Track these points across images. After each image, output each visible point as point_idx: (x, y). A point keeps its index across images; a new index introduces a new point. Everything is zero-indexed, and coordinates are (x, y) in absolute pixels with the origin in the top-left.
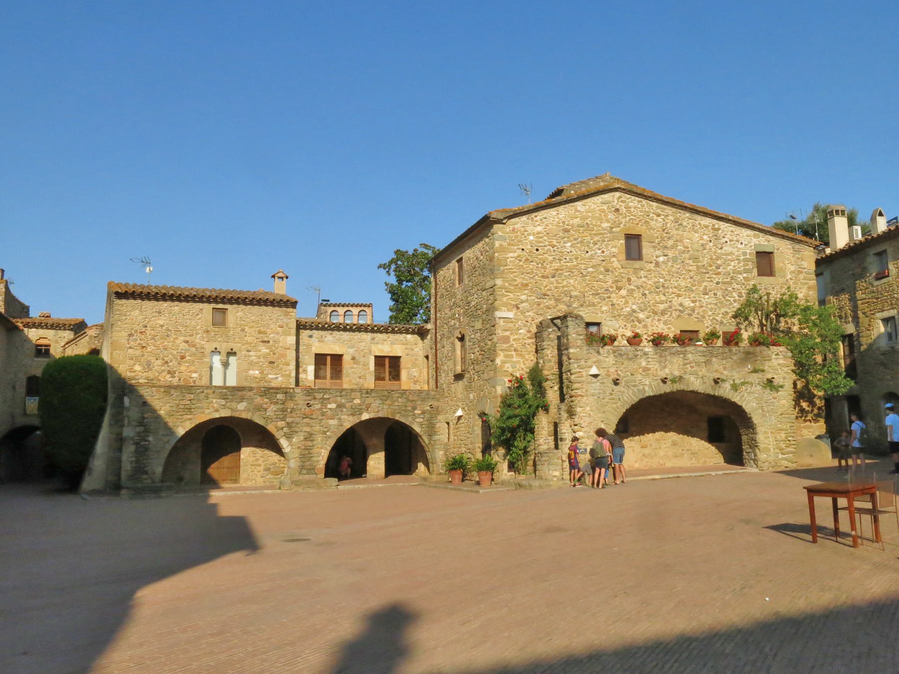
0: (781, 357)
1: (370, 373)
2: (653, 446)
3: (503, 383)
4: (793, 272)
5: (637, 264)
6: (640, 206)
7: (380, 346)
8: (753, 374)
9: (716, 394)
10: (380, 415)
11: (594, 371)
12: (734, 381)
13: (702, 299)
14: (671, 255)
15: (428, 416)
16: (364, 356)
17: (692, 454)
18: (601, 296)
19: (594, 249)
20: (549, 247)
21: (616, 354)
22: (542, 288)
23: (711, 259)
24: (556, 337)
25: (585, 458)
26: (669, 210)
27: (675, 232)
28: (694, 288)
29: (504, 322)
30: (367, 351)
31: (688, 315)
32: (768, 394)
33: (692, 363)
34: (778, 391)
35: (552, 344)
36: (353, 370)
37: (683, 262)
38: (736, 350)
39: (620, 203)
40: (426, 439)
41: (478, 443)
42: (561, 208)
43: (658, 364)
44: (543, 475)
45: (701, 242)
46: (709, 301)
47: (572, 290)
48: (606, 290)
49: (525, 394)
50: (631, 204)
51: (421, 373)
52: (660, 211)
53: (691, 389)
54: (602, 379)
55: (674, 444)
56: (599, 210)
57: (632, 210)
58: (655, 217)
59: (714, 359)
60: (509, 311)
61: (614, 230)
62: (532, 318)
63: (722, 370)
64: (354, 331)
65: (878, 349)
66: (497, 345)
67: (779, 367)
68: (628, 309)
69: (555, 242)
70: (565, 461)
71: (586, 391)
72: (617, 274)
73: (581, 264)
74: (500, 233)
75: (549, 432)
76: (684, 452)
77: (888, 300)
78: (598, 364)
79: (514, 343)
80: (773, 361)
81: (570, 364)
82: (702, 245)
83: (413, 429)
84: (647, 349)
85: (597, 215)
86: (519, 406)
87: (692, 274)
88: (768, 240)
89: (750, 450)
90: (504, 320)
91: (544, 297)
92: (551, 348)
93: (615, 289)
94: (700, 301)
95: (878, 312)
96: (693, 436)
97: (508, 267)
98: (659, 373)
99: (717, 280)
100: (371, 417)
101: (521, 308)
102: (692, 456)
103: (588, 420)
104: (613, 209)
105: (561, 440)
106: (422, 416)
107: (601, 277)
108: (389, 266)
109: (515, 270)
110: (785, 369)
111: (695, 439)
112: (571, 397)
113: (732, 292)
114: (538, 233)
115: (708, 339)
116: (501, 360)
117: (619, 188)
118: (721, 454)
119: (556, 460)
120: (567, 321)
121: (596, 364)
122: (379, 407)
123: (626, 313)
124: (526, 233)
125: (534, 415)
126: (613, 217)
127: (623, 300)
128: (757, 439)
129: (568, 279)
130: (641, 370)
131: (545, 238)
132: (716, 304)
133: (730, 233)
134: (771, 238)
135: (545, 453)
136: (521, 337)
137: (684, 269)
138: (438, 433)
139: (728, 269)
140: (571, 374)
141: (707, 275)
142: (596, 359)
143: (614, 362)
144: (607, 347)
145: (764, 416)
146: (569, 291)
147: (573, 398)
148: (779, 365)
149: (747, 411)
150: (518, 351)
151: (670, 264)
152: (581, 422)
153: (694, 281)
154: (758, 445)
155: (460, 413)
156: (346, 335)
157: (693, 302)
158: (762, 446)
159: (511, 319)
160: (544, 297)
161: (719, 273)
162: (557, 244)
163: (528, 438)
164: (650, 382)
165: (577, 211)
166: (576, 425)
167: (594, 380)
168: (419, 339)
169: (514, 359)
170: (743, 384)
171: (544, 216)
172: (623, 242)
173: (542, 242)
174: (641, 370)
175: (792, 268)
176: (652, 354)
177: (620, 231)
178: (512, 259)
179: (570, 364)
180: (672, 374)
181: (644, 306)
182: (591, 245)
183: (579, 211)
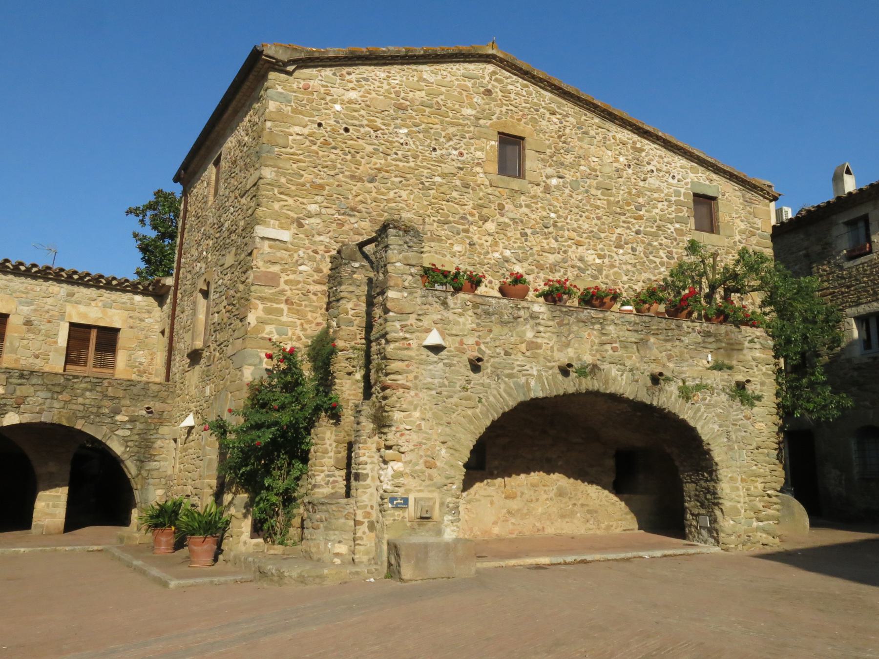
0: (758, 346)
1: (56, 350)
2: (526, 497)
3: (258, 361)
4: (741, 232)
5: (516, 184)
6: (524, 93)
7: (82, 308)
8: (714, 371)
9: (655, 404)
10: (45, 418)
11: (434, 338)
12: (684, 382)
13: (614, 255)
14: (569, 177)
15: (142, 426)
16: (49, 322)
17: (589, 512)
18: (454, 227)
19: (446, 146)
20: (367, 129)
21: (479, 311)
22: (350, 197)
23: (630, 193)
24: (365, 280)
25: (403, 517)
26: (568, 107)
27: (577, 143)
28: (603, 235)
29: (270, 247)
30: (57, 314)
31: (592, 276)
32: (736, 411)
33: (616, 342)
34: (752, 405)
35: (358, 292)
36: (25, 342)
37: (587, 192)
38: (688, 327)
39: (492, 82)
40: (131, 468)
41: (209, 477)
42: (395, 69)
43: (555, 338)
44: (314, 550)
45: (615, 164)
46: (624, 258)
47: (402, 209)
48: (462, 218)
49: (297, 383)
50: (510, 87)
51: (152, 359)
52: (555, 107)
53: (611, 389)
54: (448, 357)
55: (561, 493)
56: (458, 86)
57: (512, 96)
58: (547, 115)
59: (652, 340)
60: (282, 228)
61: (481, 122)
62: (326, 247)
63: (665, 360)
64: (34, 277)
65: (849, 361)
66: (253, 288)
67: (754, 363)
68: (497, 255)
69: (379, 123)
70: (362, 523)
71: (416, 377)
72: (481, 194)
73: (423, 167)
74: (280, 89)
75: (337, 460)
76: (575, 508)
77: (869, 289)
78: (442, 325)
79: (287, 288)
80: (745, 351)
81: (386, 320)
82: (617, 171)
83: (110, 449)
84: (536, 308)
85: (456, 93)
86: (283, 407)
87: (600, 212)
88: (711, 178)
89: (703, 511)
90: (272, 243)
91: (351, 213)
92: (355, 300)
93: (477, 218)
94: (611, 257)
95: (850, 307)
96: (591, 482)
97: (288, 150)
98: (557, 355)
99: (637, 227)
100: (24, 421)
101: (306, 226)
102: (589, 516)
103: (415, 437)
104: (482, 89)
105: (357, 477)
106: (129, 426)
107: (455, 194)
108: (144, 212)
109: (301, 157)
110: (764, 369)
111: (595, 487)
112: (384, 388)
113: (658, 249)
114: (350, 102)
115: (644, 302)
116: (258, 318)
117: (494, 57)
118: (633, 515)
119: (342, 520)
120: (387, 237)
121: (438, 325)
122: (44, 404)
123: (492, 262)
124: (329, 98)
125: (311, 424)
126: (480, 101)
127: (490, 239)
128: (719, 491)
129: (398, 188)
130: (524, 345)
131: (363, 112)
132: (634, 266)
133: (657, 158)
134: (714, 176)
135: (323, 504)
136: (301, 280)
137: (588, 202)
138: (156, 458)
139: (654, 213)
140: (388, 342)
141: (623, 218)
142: (439, 317)
143: (474, 326)
144: (461, 295)
145: (731, 449)
146: (399, 210)
147: (388, 391)
148: (754, 359)
149: (703, 438)
150: (292, 304)
151: (567, 191)
152: (400, 442)
153: (603, 224)
154: (720, 501)
155: (190, 421)
156: (19, 283)
157: (600, 257)
158: (727, 504)
159: (285, 242)
160: (351, 213)
161: (640, 218)
162: (383, 127)
163: (295, 473)
164: (538, 371)
165: (421, 79)
166: (388, 448)
167: (433, 357)
168: (156, 304)
169: (284, 319)
170: (699, 387)
171: (365, 76)
172: (494, 143)
173: (357, 119)
174: (524, 345)
175: (742, 226)
176: (545, 317)
177: (491, 125)
178: (298, 137)
179: (386, 320)
180: (579, 359)
181: (523, 253)
182: (442, 140)
183: (425, 80)
